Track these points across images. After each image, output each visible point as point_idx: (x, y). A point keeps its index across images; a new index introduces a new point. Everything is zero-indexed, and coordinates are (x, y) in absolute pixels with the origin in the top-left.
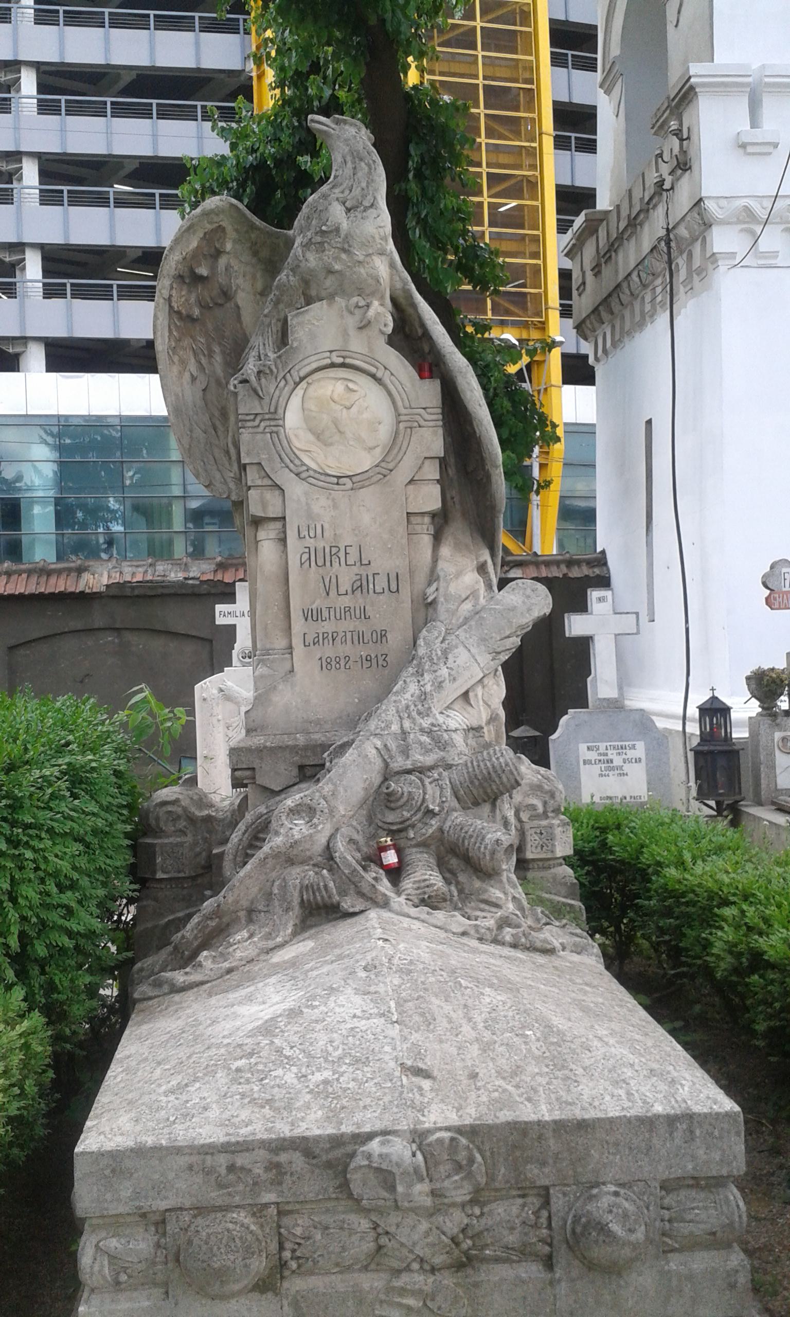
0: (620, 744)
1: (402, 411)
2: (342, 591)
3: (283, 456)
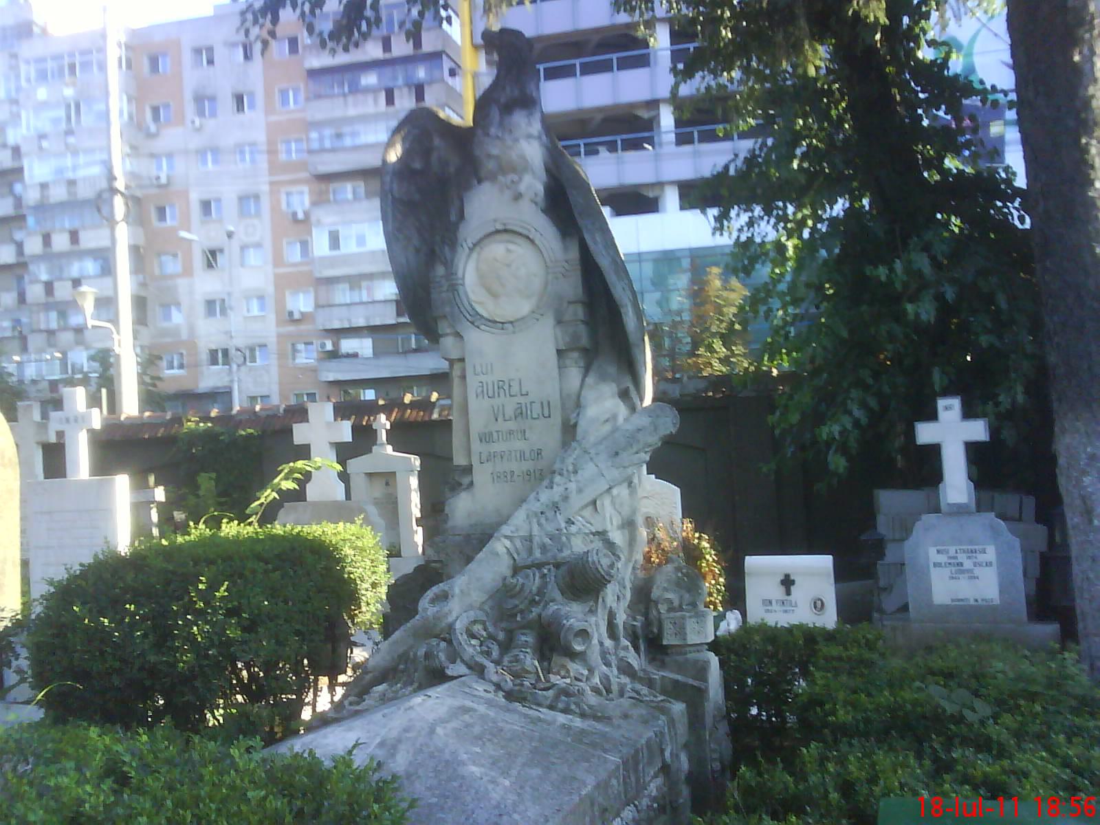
0: (970, 547)
1: (549, 264)
2: (507, 418)
3: (462, 309)
